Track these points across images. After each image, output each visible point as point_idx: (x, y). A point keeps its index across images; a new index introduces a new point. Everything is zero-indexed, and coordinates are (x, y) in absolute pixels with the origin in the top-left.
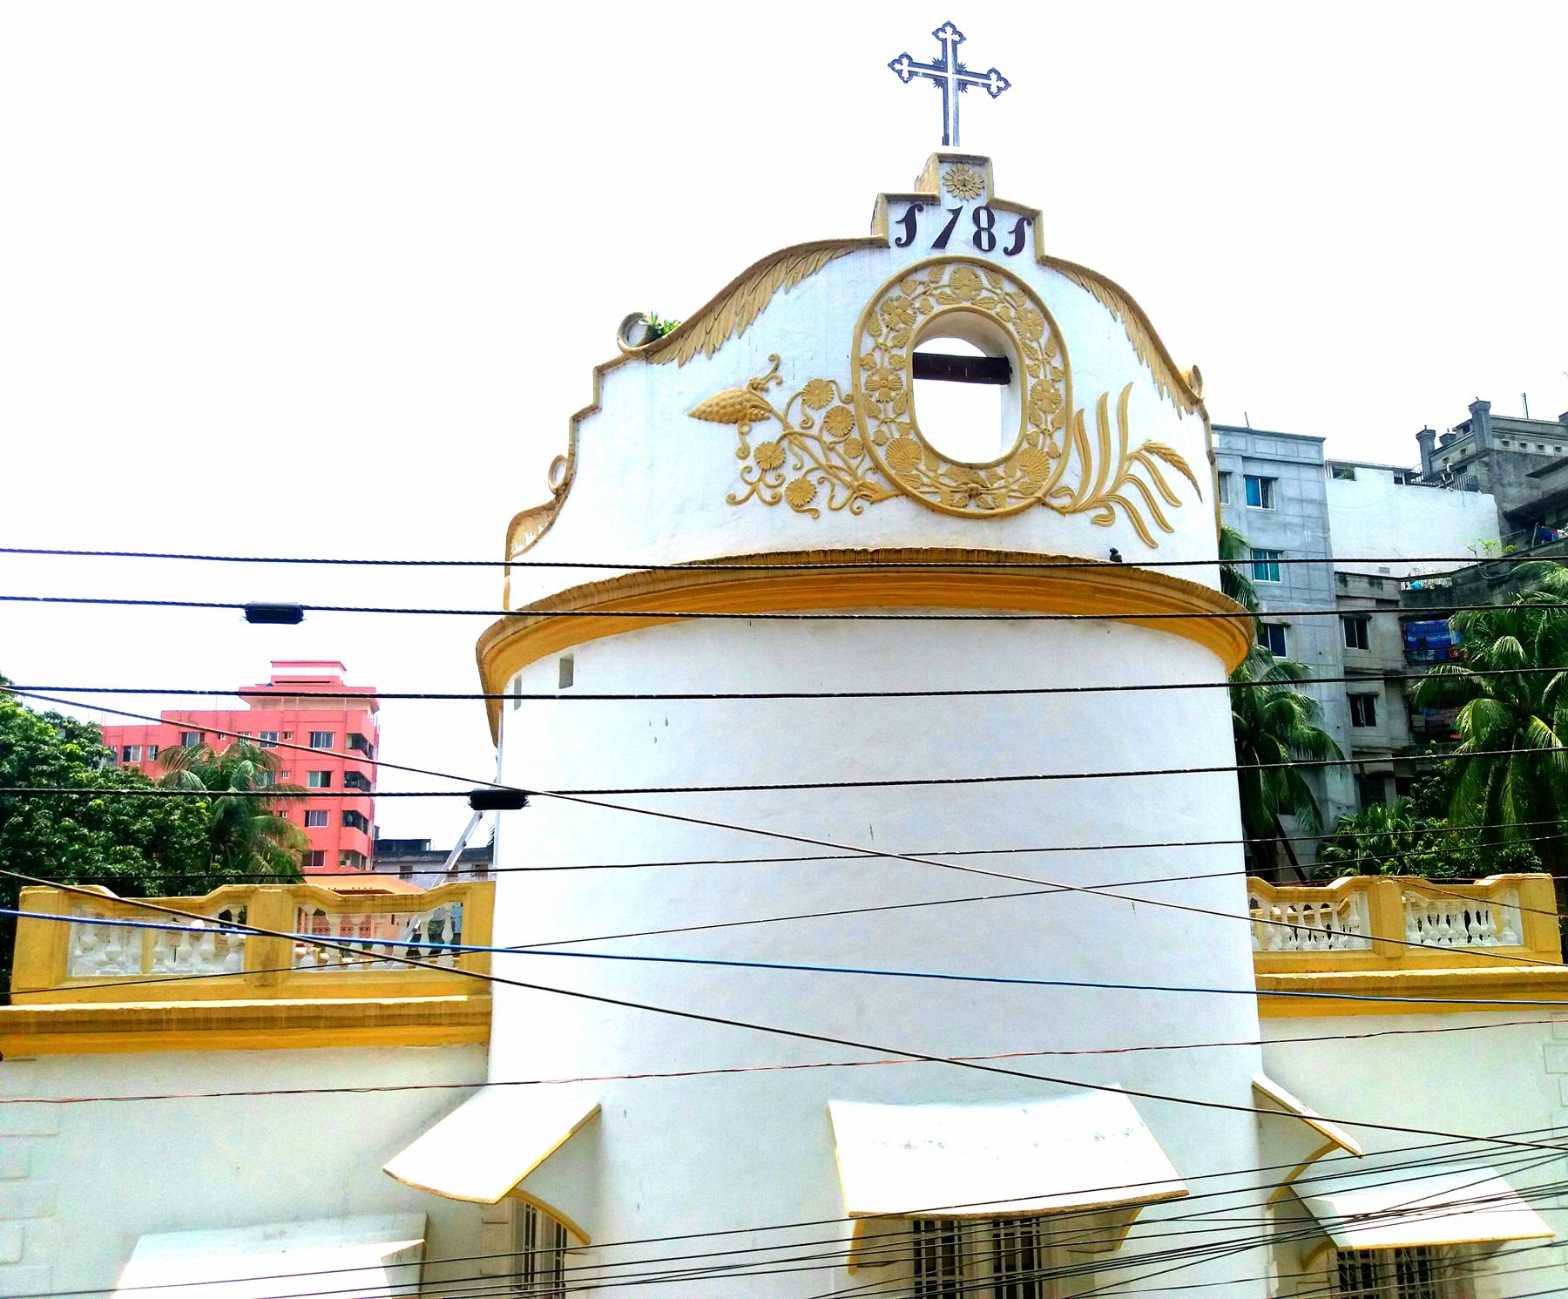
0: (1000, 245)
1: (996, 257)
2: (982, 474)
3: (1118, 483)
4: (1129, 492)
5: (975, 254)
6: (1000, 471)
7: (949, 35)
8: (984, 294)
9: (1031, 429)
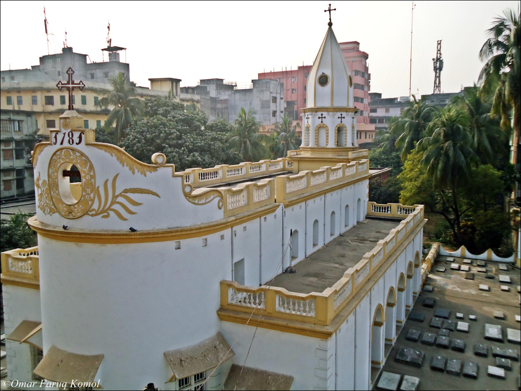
0: (75, 142)
1: (74, 146)
2: (72, 207)
3: (112, 203)
4: (116, 207)
5: (69, 145)
6: (76, 206)
7: (70, 72)
8: (72, 157)
9: (84, 194)
